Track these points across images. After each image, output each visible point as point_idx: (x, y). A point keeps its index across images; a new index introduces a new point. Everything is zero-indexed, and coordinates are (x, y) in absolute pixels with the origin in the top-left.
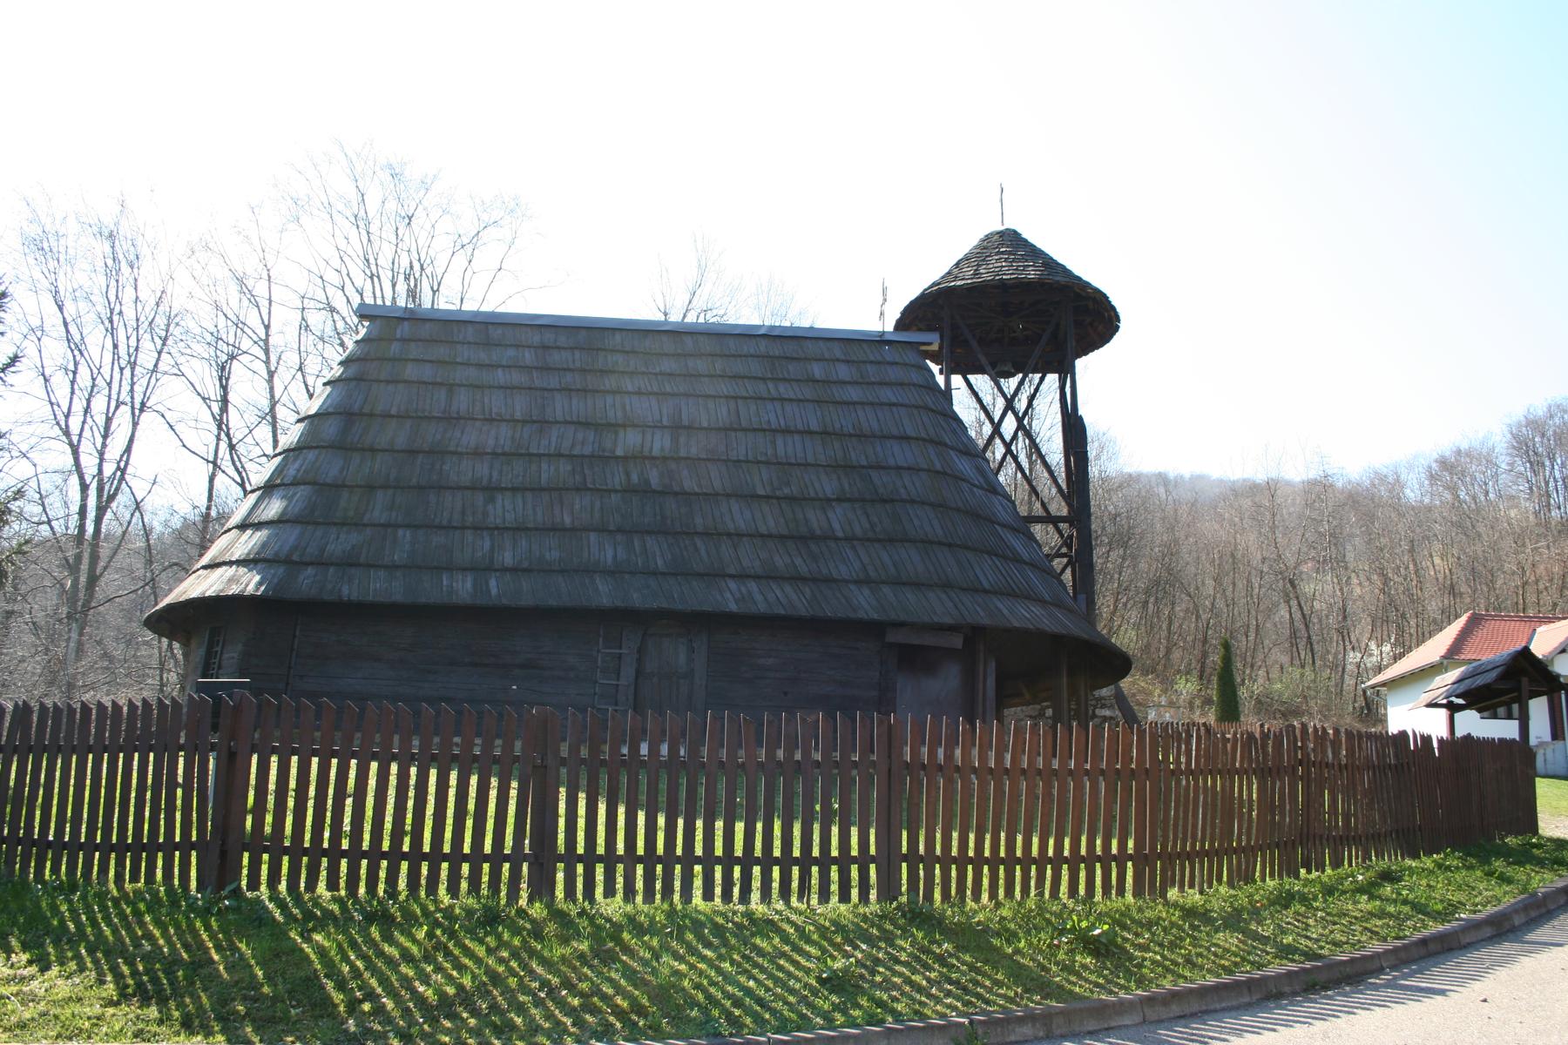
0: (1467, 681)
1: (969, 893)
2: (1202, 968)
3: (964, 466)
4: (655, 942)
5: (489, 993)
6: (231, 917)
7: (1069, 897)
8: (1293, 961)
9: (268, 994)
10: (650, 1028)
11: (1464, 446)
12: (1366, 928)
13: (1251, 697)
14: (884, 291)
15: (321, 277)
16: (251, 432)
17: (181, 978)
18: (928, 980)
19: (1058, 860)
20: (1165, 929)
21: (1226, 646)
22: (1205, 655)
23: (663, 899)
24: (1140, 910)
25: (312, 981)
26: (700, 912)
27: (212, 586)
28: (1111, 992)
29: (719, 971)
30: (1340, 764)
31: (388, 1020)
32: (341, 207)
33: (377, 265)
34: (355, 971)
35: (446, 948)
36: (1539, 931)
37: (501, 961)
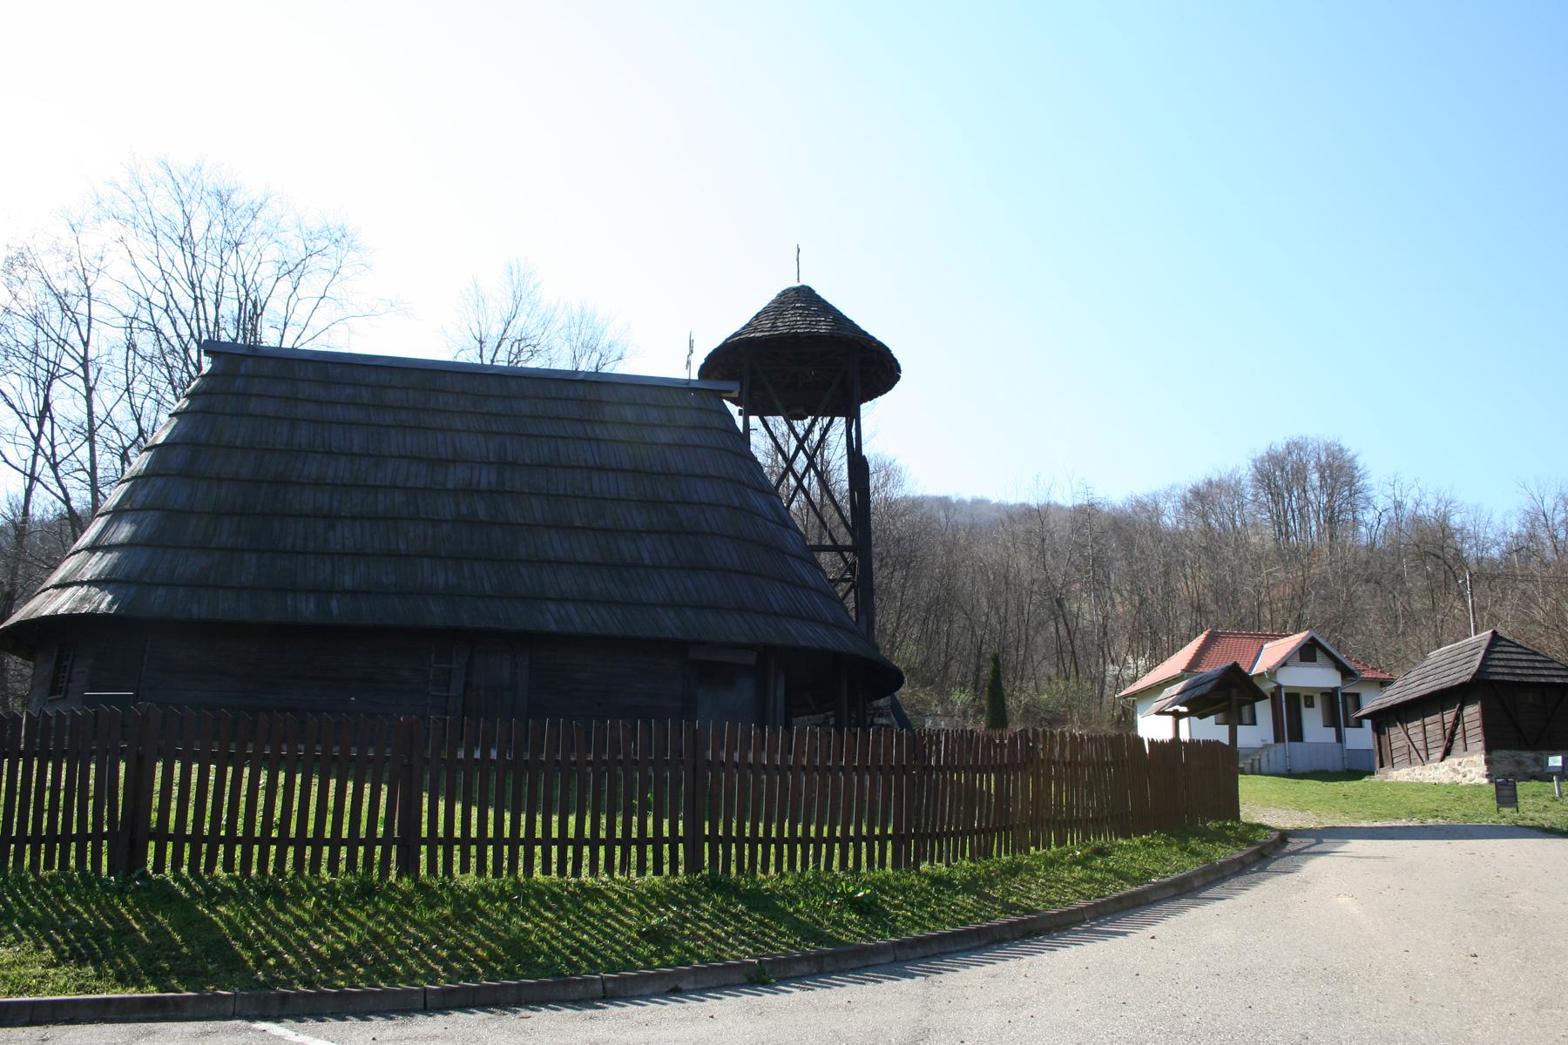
0: (1188, 692)
1: (759, 867)
2: (943, 921)
3: (759, 502)
4: (505, 907)
5: (373, 948)
6: (144, 895)
7: (841, 870)
8: (1014, 915)
9: (187, 954)
10: (506, 971)
11: (1215, 478)
12: (1076, 891)
13: (1019, 707)
14: (691, 342)
15: (148, 300)
16: (73, 452)
17: (110, 943)
18: (726, 932)
19: (831, 840)
20: (915, 893)
21: (996, 659)
22: (979, 668)
23: (509, 874)
24: (897, 879)
25: (223, 941)
26: (539, 884)
27: (64, 604)
28: (870, 940)
29: (559, 928)
30: (1064, 763)
31: (290, 970)
32: (167, 229)
33: (200, 287)
34: (259, 936)
35: (333, 916)
36: (1211, 891)
37: (380, 923)
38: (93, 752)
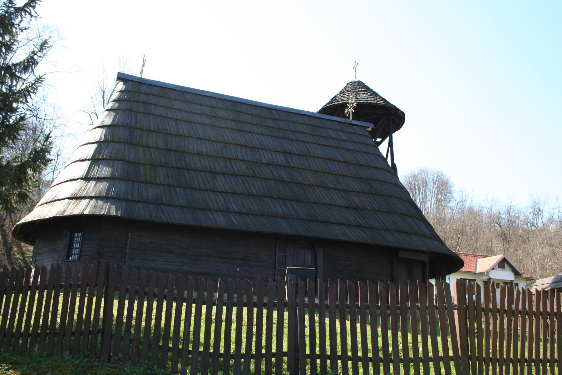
38: (61, 286)
